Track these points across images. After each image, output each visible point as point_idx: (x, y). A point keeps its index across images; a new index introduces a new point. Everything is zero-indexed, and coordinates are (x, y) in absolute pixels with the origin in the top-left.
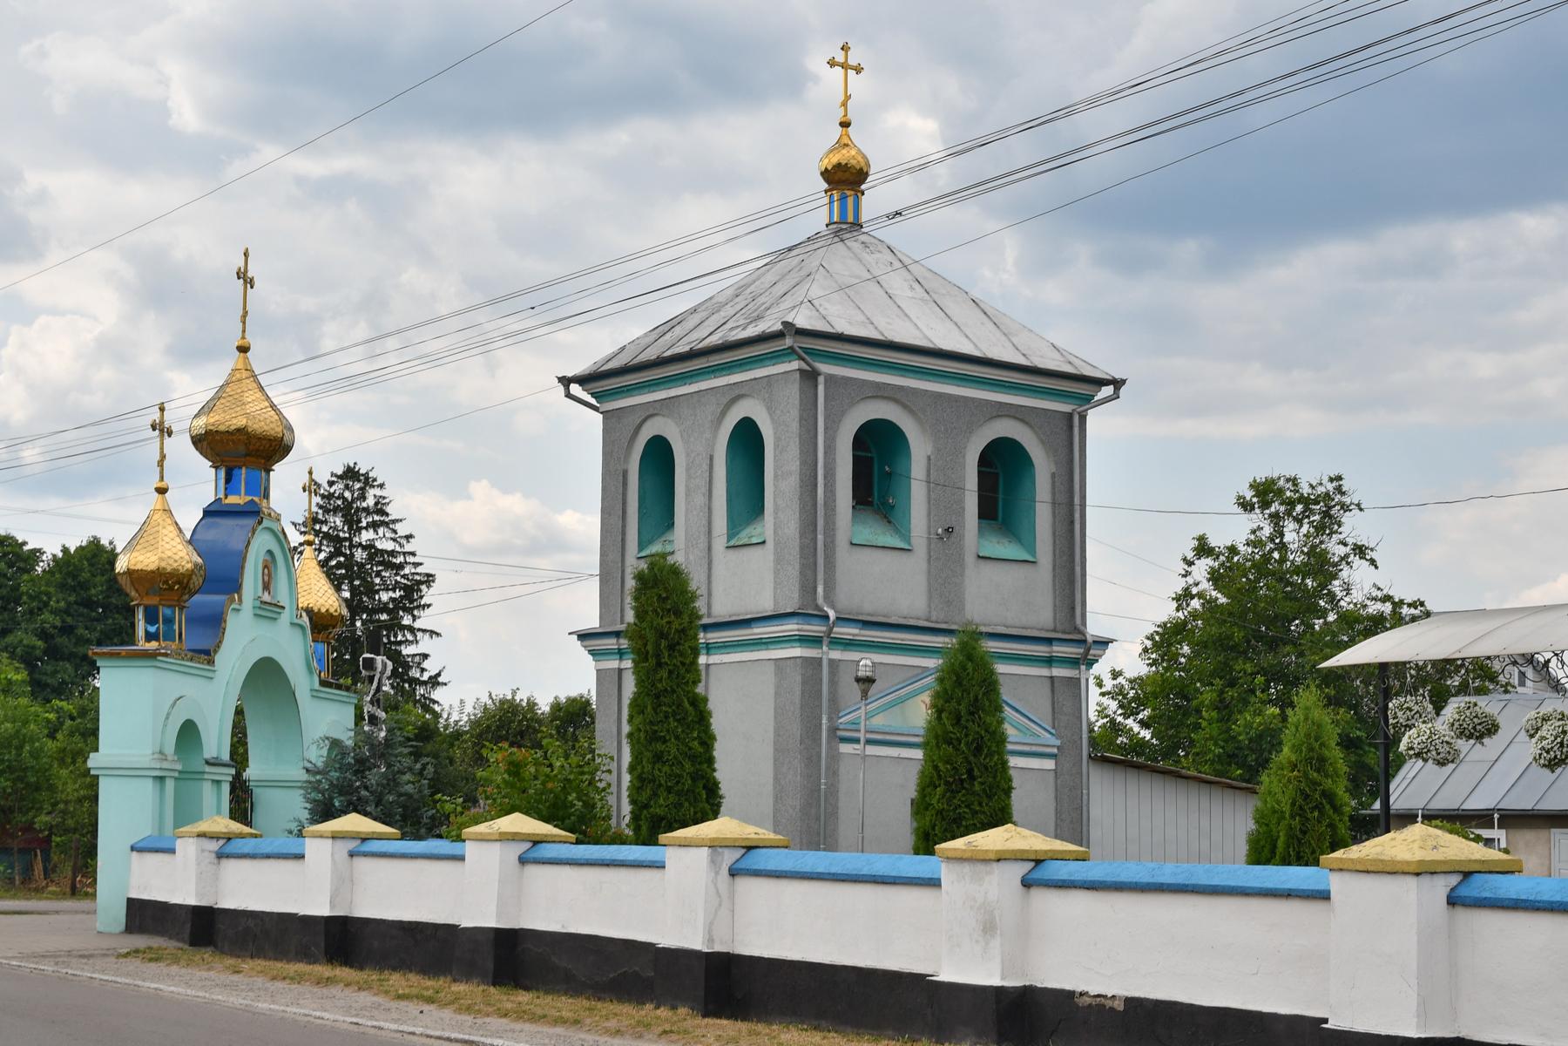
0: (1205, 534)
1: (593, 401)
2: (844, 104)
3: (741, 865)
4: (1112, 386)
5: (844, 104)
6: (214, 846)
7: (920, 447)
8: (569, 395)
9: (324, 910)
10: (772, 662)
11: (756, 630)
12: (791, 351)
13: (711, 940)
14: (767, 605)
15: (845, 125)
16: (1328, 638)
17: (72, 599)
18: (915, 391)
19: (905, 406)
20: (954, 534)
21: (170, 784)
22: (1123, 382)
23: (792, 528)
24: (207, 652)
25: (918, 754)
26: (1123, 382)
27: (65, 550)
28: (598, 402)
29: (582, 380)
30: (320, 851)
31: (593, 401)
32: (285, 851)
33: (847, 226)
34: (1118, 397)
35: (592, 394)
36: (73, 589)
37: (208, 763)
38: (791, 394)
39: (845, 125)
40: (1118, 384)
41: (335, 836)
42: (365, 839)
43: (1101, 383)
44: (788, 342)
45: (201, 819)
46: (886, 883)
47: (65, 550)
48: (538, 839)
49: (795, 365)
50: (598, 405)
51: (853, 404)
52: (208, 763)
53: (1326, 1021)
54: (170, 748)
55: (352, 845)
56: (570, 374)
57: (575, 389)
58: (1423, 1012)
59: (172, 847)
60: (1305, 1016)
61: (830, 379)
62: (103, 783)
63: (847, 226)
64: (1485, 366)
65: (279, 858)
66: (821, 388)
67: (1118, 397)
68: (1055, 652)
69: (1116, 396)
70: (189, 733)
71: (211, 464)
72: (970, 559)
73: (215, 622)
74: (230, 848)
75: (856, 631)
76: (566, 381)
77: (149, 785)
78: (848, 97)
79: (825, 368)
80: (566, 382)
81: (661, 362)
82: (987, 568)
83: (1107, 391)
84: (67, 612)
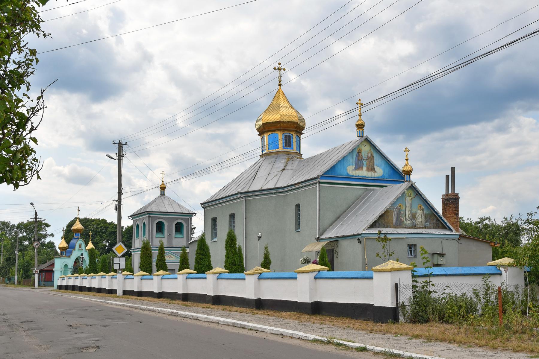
0: (458, 194)
2: (163, 179)
3: (219, 277)
5: (163, 179)
6: (62, 278)
7: (166, 224)
8: (129, 218)
9: (65, 285)
12: (146, 214)
13: (80, 284)
17: (128, 236)
18: (165, 217)
19: (164, 219)
20: (171, 235)
21: (63, 272)
23: (147, 236)
24: (69, 256)
25: (179, 264)
27: (128, 226)
29: (131, 216)
30: (180, 277)
32: (175, 277)
33: (163, 194)
36: (129, 234)
37: (69, 269)
38: (147, 219)
40: (196, 214)
41: (183, 274)
42: (127, 275)
43: (194, 214)
44: (145, 213)
45: (68, 275)
47: (128, 226)
48: (221, 273)
49: (148, 216)
52: (69, 269)
53: (298, 301)
54: (63, 267)
55: (68, 278)
56: (129, 216)
57: (130, 217)
58: (158, 291)
59: (176, 277)
60: (239, 297)
61: (152, 217)
62: (55, 272)
63: (163, 194)
64: (470, 159)
65: (230, 279)
66: (151, 218)
69: (195, 215)
70: (66, 266)
72: (173, 238)
73: (71, 252)
74: (114, 277)
76: (129, 217)
77: (59, 272)
78: (163, 178)
79: (151, 216)
81: (138, 214)
82: (176, 239)
83: (194, 214)
84: (128, 238)
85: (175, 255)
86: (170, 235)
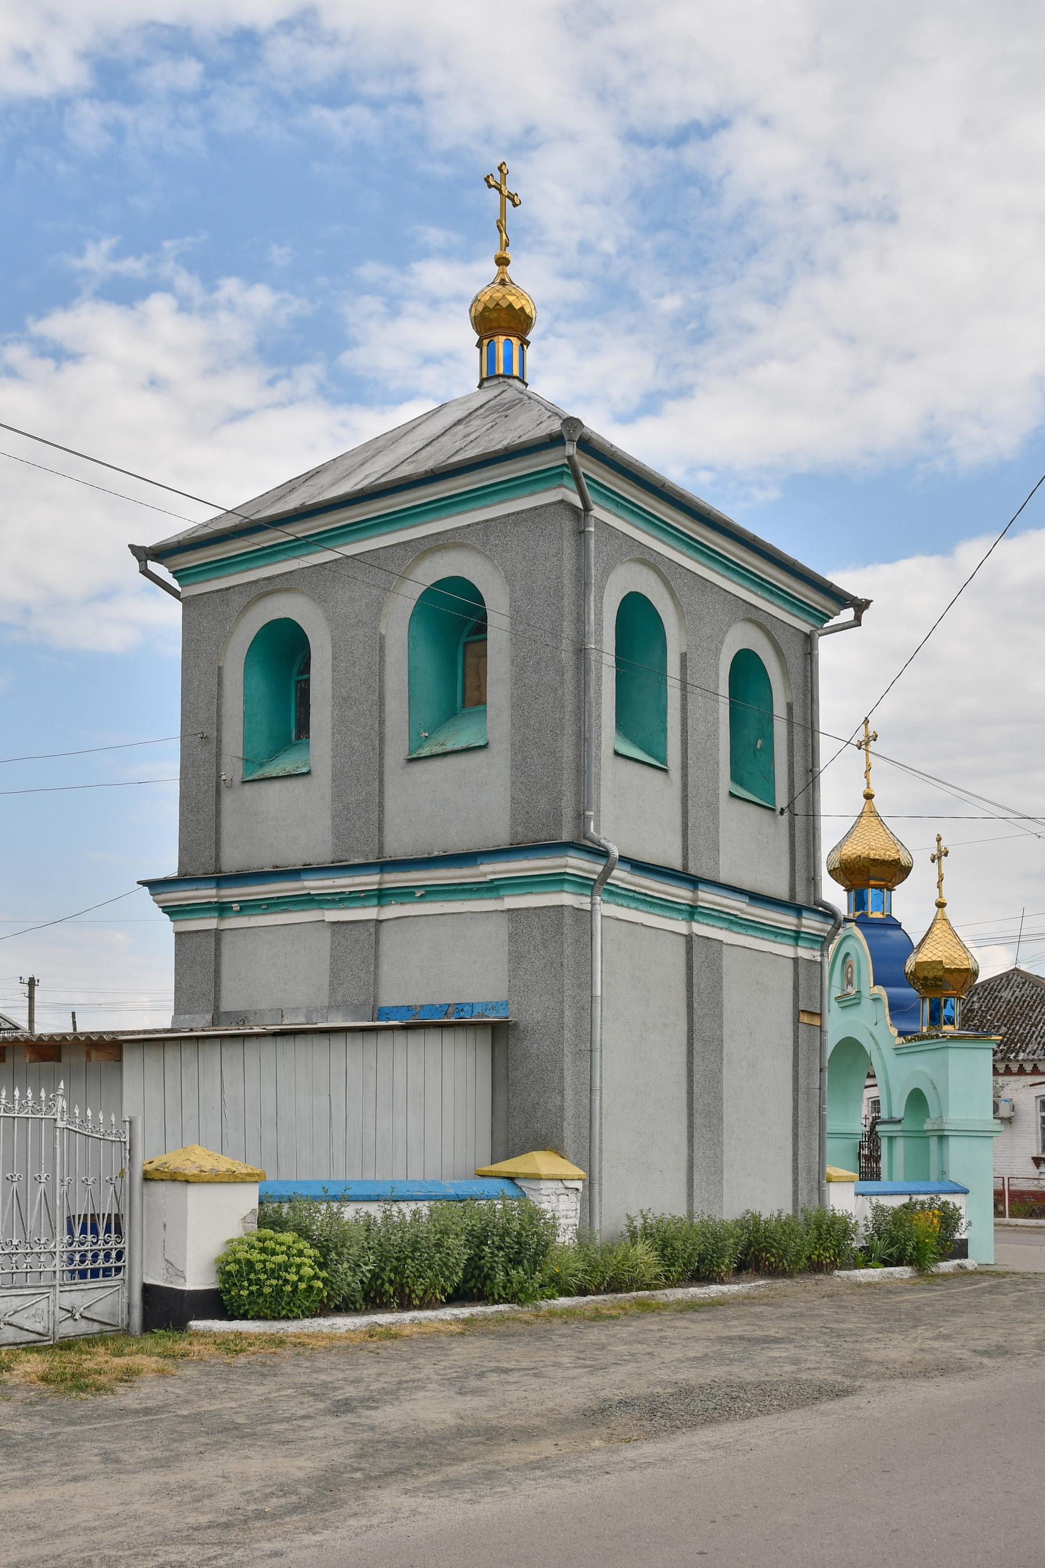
1: (175, 584)
4: (852, 609)
8: (146, 572)
10: (505, 915)
11: (307, 884)
14: (322, 852)
15: (941, 905)
16: (378, 1301)
22: (867, 603)
26: (867, 603)
28: (180, 586)
29: (161, 553)
31: (175, 584)
34: (860, 625)
35: (174, 573)
39: (941, 905)
46: (359, 1201)
50: (179, 589)
51: (510, 580)
56: (149, 541)
67: (860, 625)
68: (702, 901)
71: (844, 888)
75: (376, 878)
76: (143, 554)
80: (144, 556)
83: (848, 614)
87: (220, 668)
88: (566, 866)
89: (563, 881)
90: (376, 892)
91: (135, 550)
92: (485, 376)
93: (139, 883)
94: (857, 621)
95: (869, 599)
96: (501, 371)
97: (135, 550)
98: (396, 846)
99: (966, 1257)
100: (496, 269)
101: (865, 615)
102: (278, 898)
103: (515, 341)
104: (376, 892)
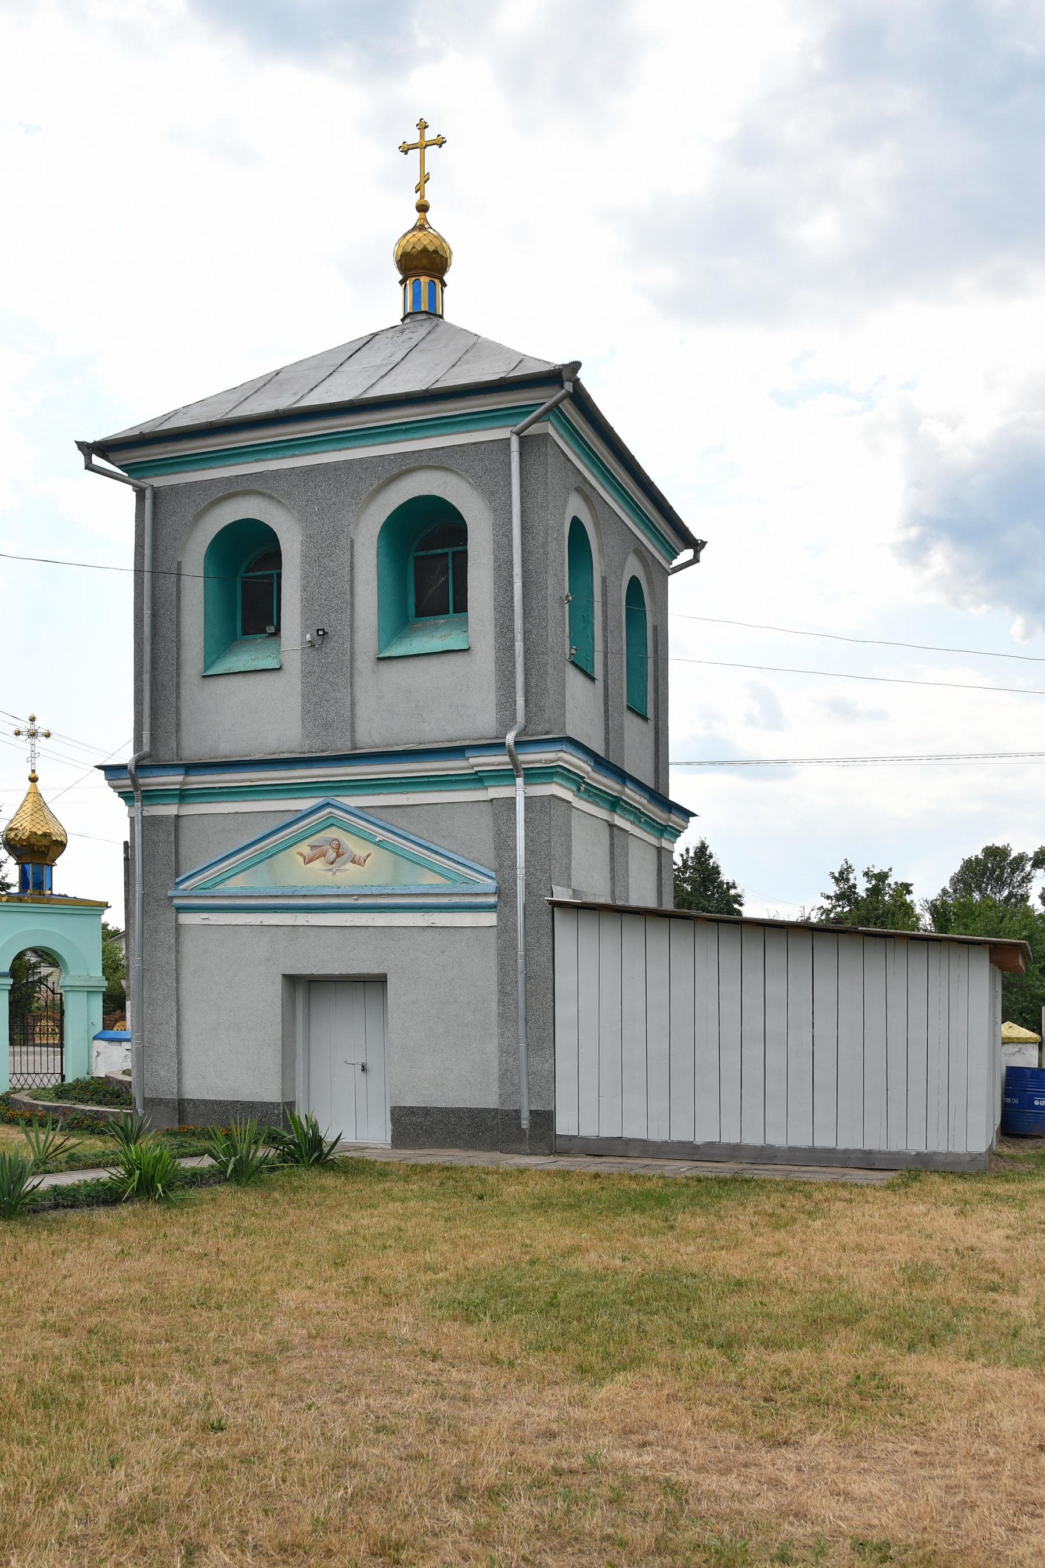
8: (89, 467)
11: (472, 761)
22: (703, 544)
26: (703, 544)
29: (105, 448)
56: (92, 437)
72: (364, 662)
76: (87, 449)
83: (687, 554)
85: (381, 835)
86: (323, 634)
87: (352, 541)
88: (558, 760)
89: (552, 775)
90: (178, 792)
91: (81, 446)
92: (408, 310)
93: (96, 767)
94: (695, 560)
95: (704, 540)
96: (424, 307)
97: (81, 446)
98: (369, 736)
99: (518, 1112)
100: (417, 215)
101: (703, 554)
102: (220, 788)
103: (437, 282)
104: (178, 792)
